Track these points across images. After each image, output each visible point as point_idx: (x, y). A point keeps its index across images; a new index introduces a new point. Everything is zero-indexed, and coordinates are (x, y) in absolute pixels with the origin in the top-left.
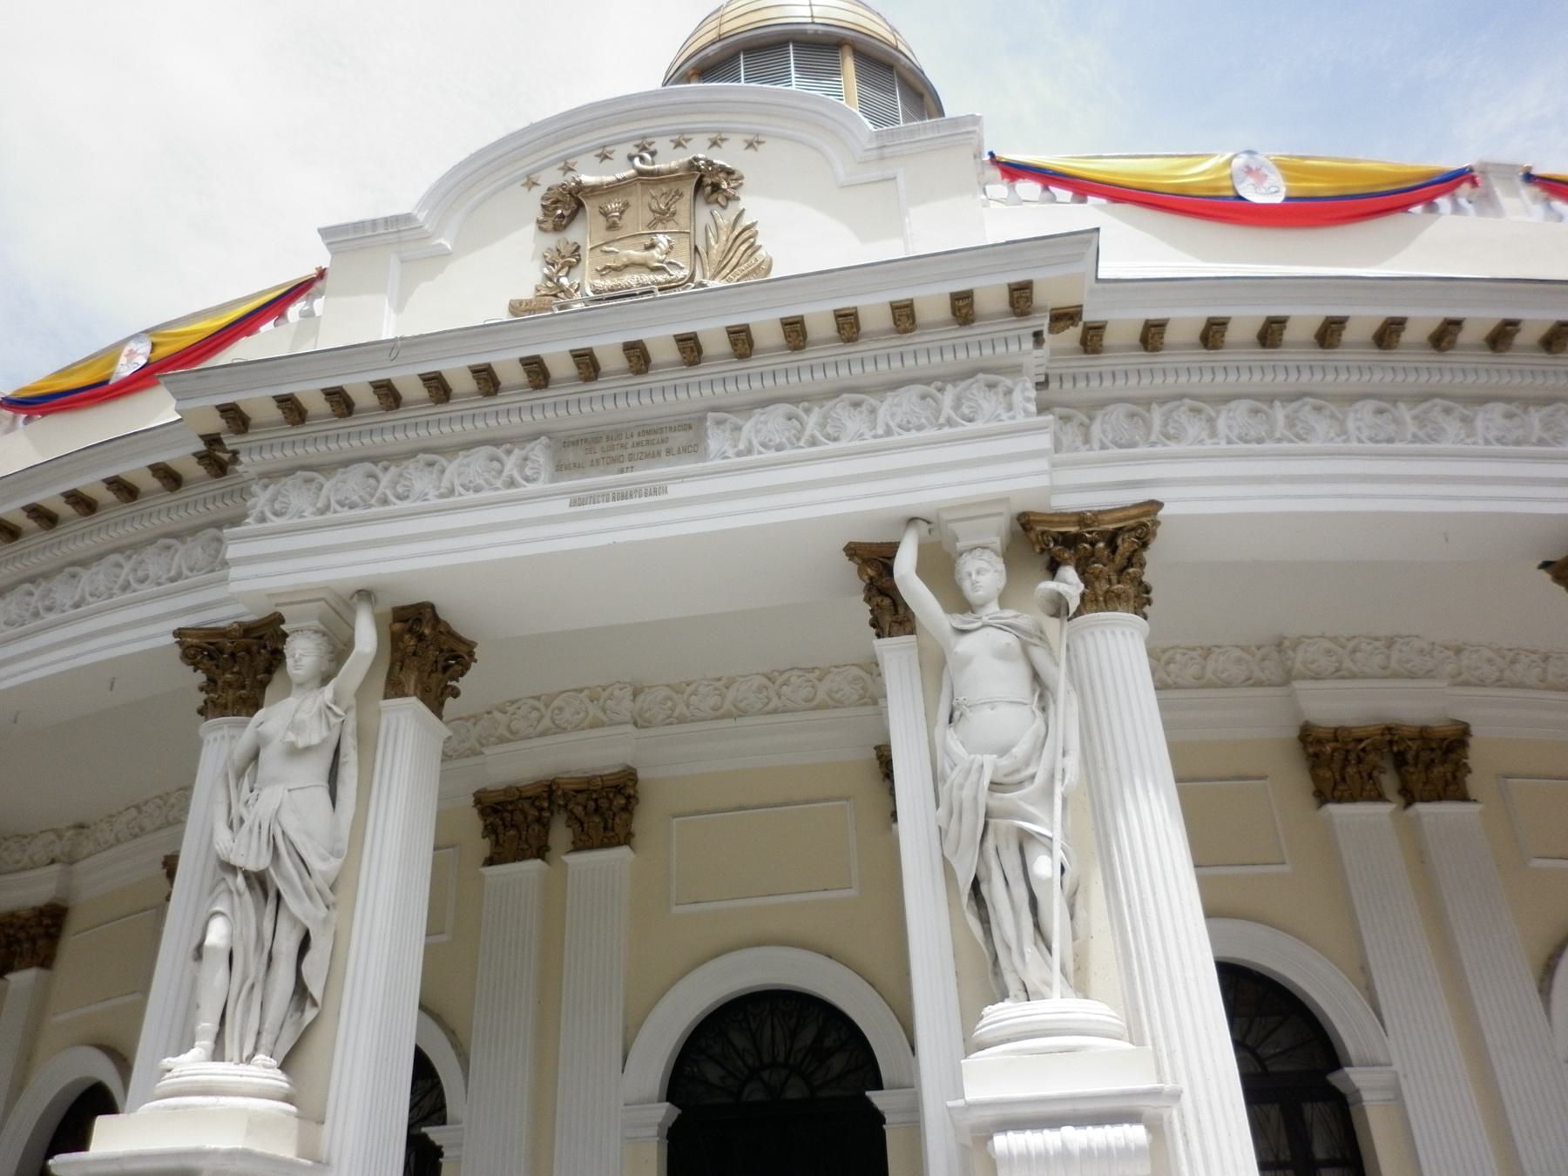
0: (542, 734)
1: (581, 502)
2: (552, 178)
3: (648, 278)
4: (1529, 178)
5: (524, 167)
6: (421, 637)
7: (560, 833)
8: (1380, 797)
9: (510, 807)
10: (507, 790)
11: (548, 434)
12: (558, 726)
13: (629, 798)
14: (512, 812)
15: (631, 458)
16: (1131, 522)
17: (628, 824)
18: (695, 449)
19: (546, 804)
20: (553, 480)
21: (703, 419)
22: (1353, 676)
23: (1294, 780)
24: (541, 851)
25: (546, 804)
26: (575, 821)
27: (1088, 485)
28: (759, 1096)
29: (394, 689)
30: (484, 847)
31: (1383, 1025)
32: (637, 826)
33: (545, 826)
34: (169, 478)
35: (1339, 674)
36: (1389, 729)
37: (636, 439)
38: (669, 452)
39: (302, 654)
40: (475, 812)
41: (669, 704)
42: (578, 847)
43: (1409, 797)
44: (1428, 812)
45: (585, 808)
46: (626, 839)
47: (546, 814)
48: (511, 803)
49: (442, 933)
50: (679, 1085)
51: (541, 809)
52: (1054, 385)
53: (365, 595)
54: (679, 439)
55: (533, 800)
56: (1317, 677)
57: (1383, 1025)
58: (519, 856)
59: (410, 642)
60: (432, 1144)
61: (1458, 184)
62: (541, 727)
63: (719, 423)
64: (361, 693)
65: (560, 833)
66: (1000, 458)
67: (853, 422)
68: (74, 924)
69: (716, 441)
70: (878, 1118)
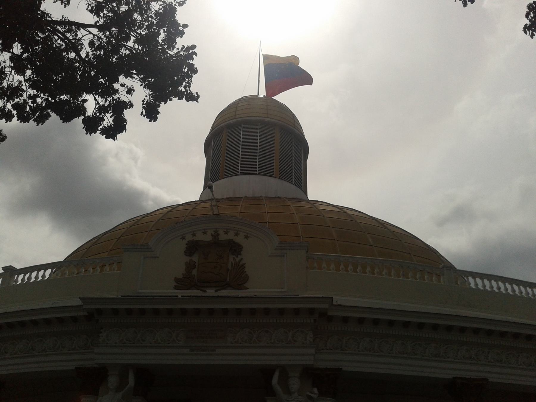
2: (189, 238)
39: (113, 381)
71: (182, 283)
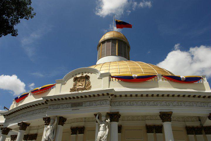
0: (77, 122)
1: (73, 110)
3: (81, 87)
4: (162, 76)
5: (72, 75)
7: (78, 132)
8: (153, 133)
11: (71, 103)
16: (128, 106)
17: (83, 131)
18: (82, 105)
20: (71, 108)
22: (152, 120)
23: (145, 130)
24: (76, 134)
27: (114, 109)
29: (59, 124)
30: (71, 133)
33: (76, 131)
34: (43, 104)
35: (151, 120)
36: (154, 125)
42: (79, 134)
43: (156, 133)
44: (157, 134)
46: (83, 133)
52: (112, 100)
54: (81, 104)
55: (76, 128)
56: (148, 120)
65: (78, 132)
66: (106, 109)
67: (94, 104)
68: (38, 135)
71: (72, 90)
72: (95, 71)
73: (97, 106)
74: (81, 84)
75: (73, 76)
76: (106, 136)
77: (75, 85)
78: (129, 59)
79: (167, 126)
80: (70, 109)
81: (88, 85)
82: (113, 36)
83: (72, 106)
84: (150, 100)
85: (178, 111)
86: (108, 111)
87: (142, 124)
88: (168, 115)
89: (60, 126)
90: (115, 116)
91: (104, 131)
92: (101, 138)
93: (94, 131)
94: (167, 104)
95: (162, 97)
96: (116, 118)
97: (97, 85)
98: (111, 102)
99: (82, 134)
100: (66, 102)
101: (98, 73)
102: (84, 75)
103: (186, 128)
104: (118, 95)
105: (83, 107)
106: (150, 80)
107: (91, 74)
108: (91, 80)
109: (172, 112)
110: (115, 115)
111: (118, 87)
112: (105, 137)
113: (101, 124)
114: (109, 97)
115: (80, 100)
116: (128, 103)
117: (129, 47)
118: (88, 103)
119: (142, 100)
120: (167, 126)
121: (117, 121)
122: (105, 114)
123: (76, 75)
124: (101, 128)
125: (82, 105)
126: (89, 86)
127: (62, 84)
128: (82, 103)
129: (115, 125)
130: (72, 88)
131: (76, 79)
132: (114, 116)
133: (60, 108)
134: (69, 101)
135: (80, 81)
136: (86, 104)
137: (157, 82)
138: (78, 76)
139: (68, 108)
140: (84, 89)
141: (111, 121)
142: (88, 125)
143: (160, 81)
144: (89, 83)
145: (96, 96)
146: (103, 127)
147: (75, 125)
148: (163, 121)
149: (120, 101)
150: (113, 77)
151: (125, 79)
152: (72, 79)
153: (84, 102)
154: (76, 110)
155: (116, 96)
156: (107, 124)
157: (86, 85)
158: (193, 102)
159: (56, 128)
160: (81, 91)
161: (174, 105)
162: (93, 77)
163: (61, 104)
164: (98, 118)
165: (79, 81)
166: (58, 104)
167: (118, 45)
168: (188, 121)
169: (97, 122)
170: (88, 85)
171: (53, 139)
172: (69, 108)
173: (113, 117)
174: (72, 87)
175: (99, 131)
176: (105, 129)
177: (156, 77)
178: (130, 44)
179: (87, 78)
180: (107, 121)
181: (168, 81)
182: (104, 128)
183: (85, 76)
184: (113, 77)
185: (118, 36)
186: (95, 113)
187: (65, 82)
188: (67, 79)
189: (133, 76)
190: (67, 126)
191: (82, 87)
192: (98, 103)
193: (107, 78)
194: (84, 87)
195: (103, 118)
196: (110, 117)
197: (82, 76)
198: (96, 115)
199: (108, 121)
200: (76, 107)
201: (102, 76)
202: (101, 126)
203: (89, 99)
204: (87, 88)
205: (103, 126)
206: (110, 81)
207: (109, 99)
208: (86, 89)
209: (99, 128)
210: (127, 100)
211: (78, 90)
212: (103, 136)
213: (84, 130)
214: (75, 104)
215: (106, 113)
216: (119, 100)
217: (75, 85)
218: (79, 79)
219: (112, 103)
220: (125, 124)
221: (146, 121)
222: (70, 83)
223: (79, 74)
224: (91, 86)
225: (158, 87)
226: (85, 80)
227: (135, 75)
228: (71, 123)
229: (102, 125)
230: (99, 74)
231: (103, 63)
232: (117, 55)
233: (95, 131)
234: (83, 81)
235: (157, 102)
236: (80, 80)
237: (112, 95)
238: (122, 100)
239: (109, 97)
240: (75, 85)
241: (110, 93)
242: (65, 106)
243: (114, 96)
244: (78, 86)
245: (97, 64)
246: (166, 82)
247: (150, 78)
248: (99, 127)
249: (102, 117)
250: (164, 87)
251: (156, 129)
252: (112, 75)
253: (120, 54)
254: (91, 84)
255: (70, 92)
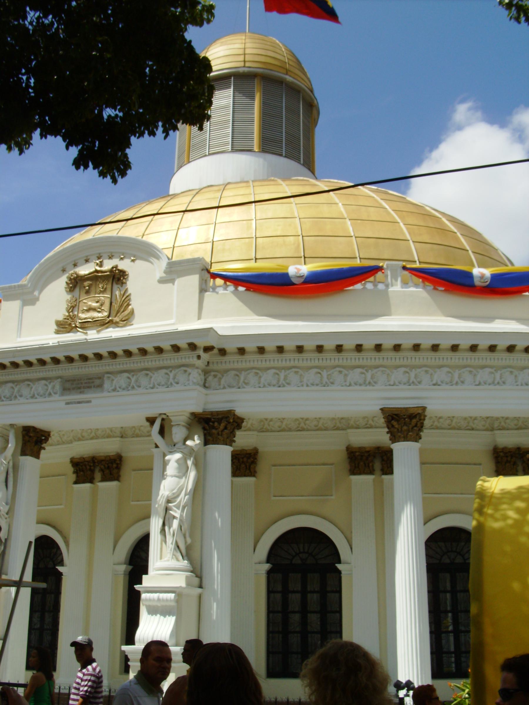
0: (92, 439)
1: (67, 404)
3: (96, 315)
6: (30, 437)
7: (98, 475)
9: (81, 464)
10: (80, 458)
12: (97, 436)
13: (117, 464)
14: (82, 466)
15: (84, 388)
18: (100, 386)
19: (92, 465)
20: (62, 395)
21: (104, 376)
24: (91, 481)
25: (92, 465)
26: (102, 470)
27: (218, 401)
28: (299, 562)
30: (73, 477)
31: (114, 550)
32: (122, 473)
33: (93, 471)
37: (85, 381)
38: (94, 387)
40: (70, 465)
41: (134, 429)
45: (104, 466)
46: (117, 478)
47: (92, 468)
48: (82, 463)
49: (61, 505)
50: (273, 554)
51: (91, 466)
52: (211, 365)
53: (12, 426)
54: (97, 382)
57: (114, 550)
58: (84, 482)
59: (27, 438)
60: (59, 572)
61: (377, 273)
62: (91, 436)
63: (109, 377)
64: (14, 455)
65: (98, 475)
66: (185, 399)
67: (144, 381)
69: (107, 385)
70: (339, 572)
71: (64, 326)
72: (144, 251)
73: (155, 390)
74: (95, 305)
75: (64, 271)
76: (185, 495)
77: (73, 307)
78: (309, 165)
79: (405, 453)
80: (58, 402)
81: (121, 306)
82: (241, 58)
83: (65, 390)
84: (349, 363)
85: (440, 400)
86: (198, 409)
87: (335, 445)
88: (412, 416)
89: (28, 461)
90: (220, 424)
91: (180, 477)
92: (169, 501)
93: (150, 472)
94: (412, 379)
95: (393, 354)
96: (222, 431)
97: (160, 310)
98: (206, 373)
99: (114, 483)
100: (41, 375)
101: (158, 258)
102: (108, 265)
103: (494, 454)
104: (231, 347)
105: (105, 394)
106: (359, 286)
107: (133, 261)
108: (132, 285)
109: (424, 409)
110: (220, 421)
111: (235, 319)
112: (183, 498)
113: (171, 453)
114: (199, 357)
115: (93, 368)
116: (268, 376)
117: (311, 107)
118: (121, 380)
119: (321, 363)
120: (405, 453)
121: (229, 441)
122: (184, 418)
123: (75, 265)
124: (171, 469)
125: (100, 386)
126: (126, 312)
127: (25, 303)
128: (100, 377)
129: (221, 455)
130: (61, 318)
131: (75, 283)
132: (216, 426)
133: (21, 396)
134: (52, 371)
135: (93, 289)
136: (114, 382)
137: (385, 293)
138: (84, 270)
139: (50, 394)
140: (103, 324)
141: (206, 443)
142: (133, 450)
143: (396, 288)
144: (126, 300)
145: (151, 353)
146: (176, 465)
147: (85, 449)
148: (394, 439)
149: (240, 370)
150: (214, 276)
151: (267, 285)
152: (62, 282)
153: (106, 375)
154: (79, 403)
155: (223, 352)
156: (190, 453)
157: (116, 306)
158: (505, 367)
159: (16, 468)
160: (98, 332)
161: (434, 382)
162: (141, 278)
163: (23, 381)
164: (162, 432)
165: (88, 292)
166: (13, 382)
167: (265, 105)
168: (503, 429)
169: (157, 446)
170: (121, 306)
171: (7, 504)
172: (56, 397)
173: (214, 427)
174: (61, 314)
175: (163, 476)
176: (183, 471)
177: (379, 274)
178: (321, 96)
179: (118, 277)
180: (189, 443)
181: (424, 287)
182: (179, 468)
183: (111, 271)
184: (214, 276)
185: (263, 59)
186: (151, 413)
187: (36, 293)
188: (42, 280)
189: (292, 270)
190: (56, 456)
191: (100, 315)
192: (159, 377)
193: (193, 281)
194: (106, 314)
195: (178, 433)
196: (204, 429)
197: (97, 271)
198: (151, 421)
199: (195, 442)
200: (81, 393)
201: (176, 269)
202: (169, 461)
203: (123, 363)
204: (117, 319)
205: (177, 461)
206: (203, 290)
207: (200, 363)
208: (116, 324)
209: (164, 469)
210: (264, 365)
211: (85, 325)
212: (178, 496)
213: (119, 468)
214: (74, 380)
215: (188, 415)
216: (236, 366)
217: (73, 307)
218: (86, 283)
219: (209, 377)
220: (269, 445)
221: (349, 431)
222: (56, 297)
223: (87, 261)
224: (132, 312)
225: (385, 312)
226: (109, 286)
227: (299, 269)
228: (71, 442)
229: (174, 458)
230: (163, 264)
231: (197, 187)
232: (256, 149)
233: (152, 469)
234: (104, 291)
235: (375, 371)
236: (90, 286)
237: (208, 349)
238: (248, 365)
239: (199, 357)
240: (72, 308)
241: (201, 343)
242: (39, 387)
243: (215, 351)
244: (84, 311)
245: (171, 192)
246: (418, 291)
247: (372, 272)
248: (165, 464)
249: (175, 430)
250: (413, 314)
251: (383, 460)
252: (215, 269)
253: (269, 145)
254: (135, 304)
255: (57, 332)
